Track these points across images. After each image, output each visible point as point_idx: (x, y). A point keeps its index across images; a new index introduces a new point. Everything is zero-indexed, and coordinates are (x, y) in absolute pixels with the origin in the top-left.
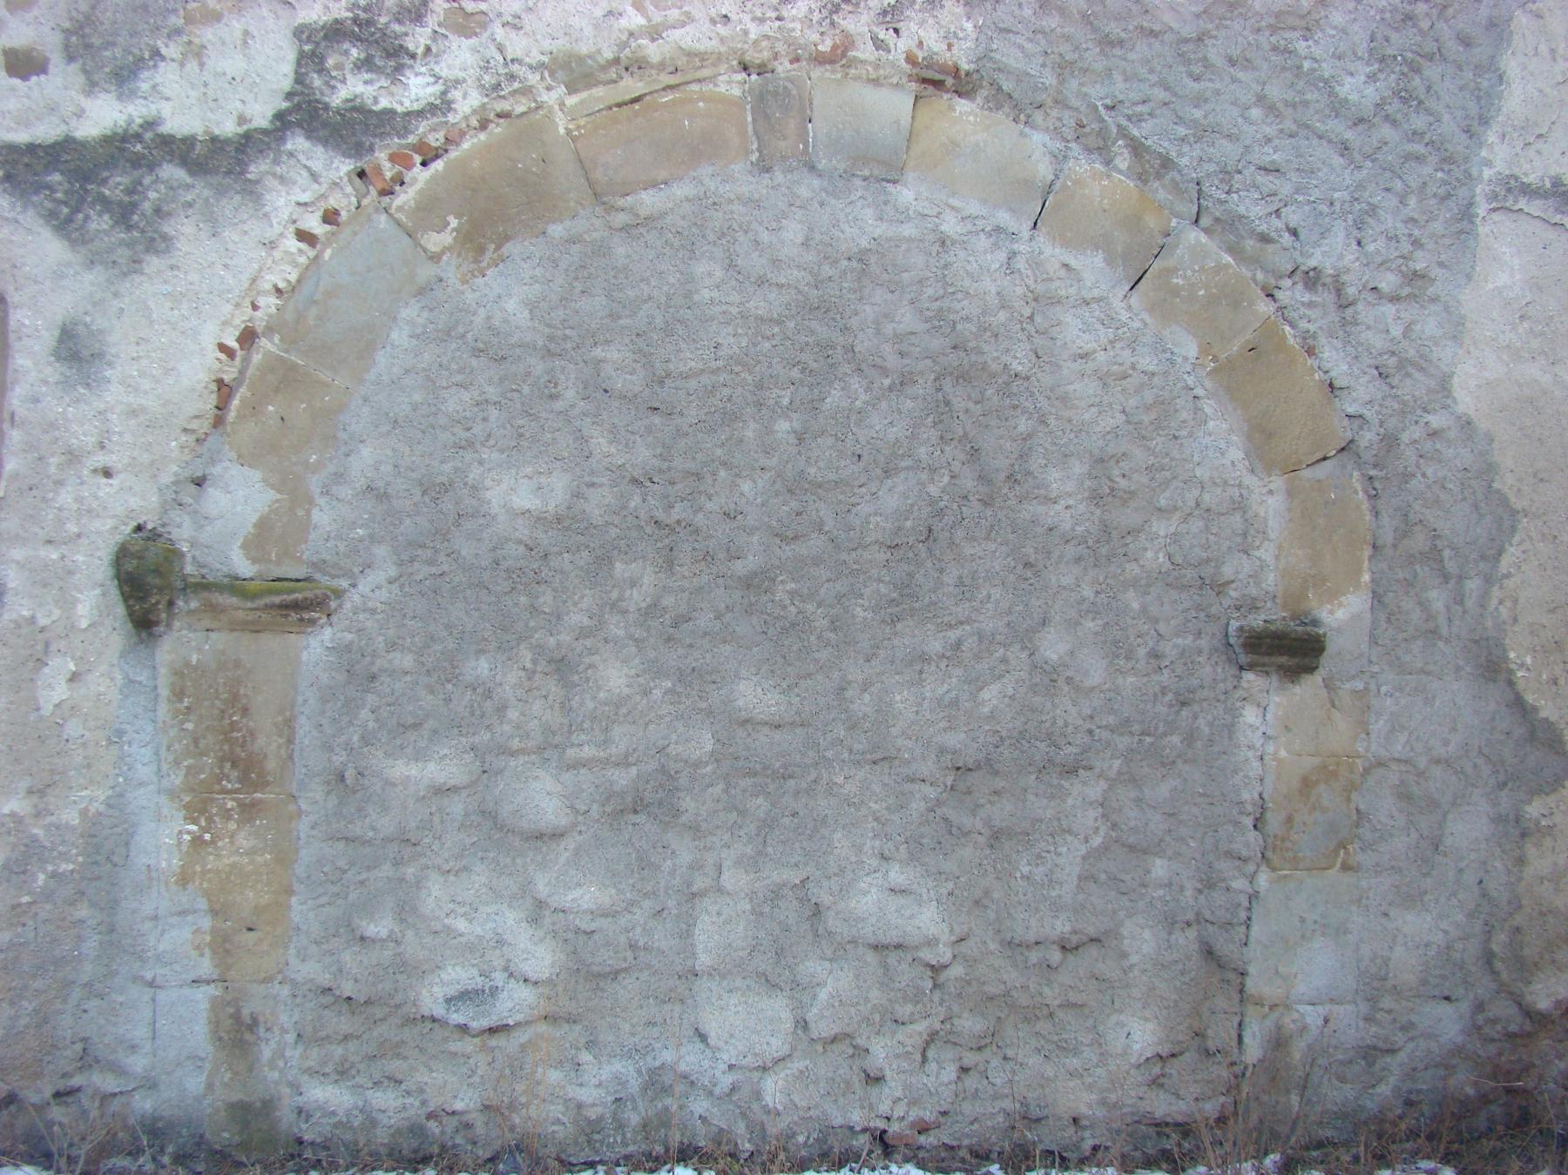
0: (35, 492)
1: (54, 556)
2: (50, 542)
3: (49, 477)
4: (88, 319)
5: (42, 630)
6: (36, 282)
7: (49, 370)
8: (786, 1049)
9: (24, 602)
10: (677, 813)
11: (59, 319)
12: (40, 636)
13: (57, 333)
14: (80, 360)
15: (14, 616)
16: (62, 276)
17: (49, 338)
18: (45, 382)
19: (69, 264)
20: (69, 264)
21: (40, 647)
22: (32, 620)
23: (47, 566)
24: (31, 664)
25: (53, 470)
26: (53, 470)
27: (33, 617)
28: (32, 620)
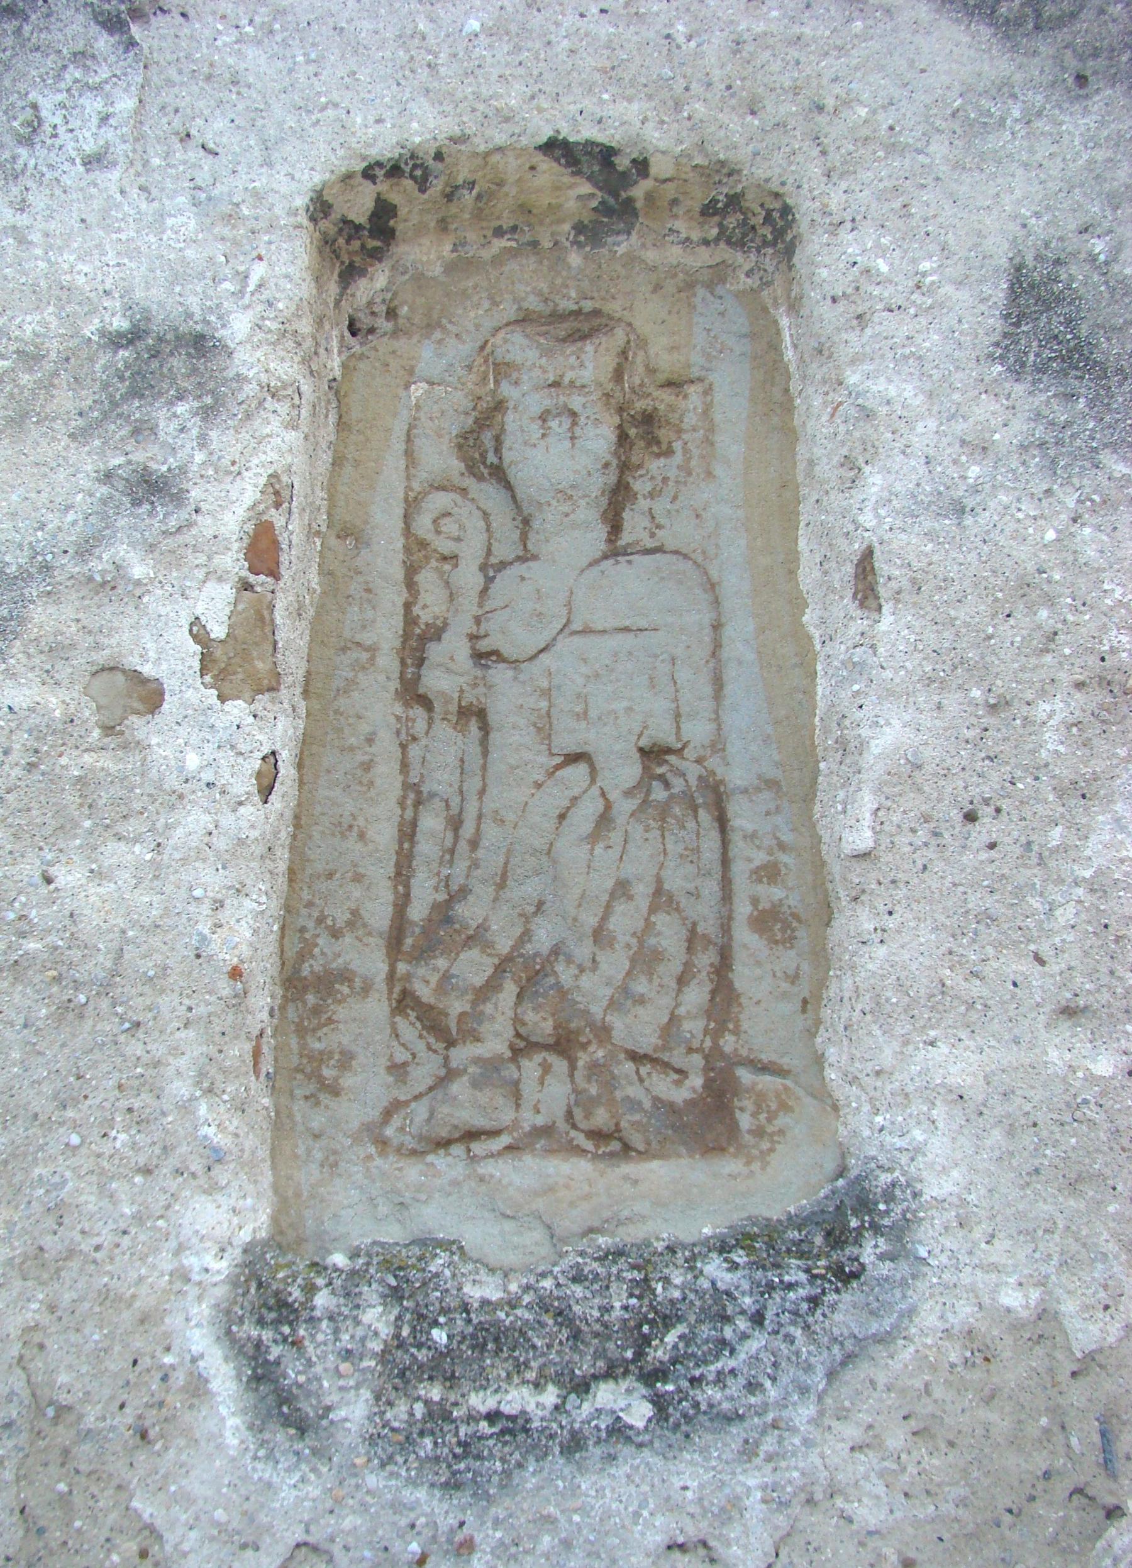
0: (987, 828)
1: (1104, 1066)
2: (1069, 1012)
3: (1036, 771)
4: (1099, 246)
5: (1087, 1365)
6: (892, 149)
7: (986, 409)
8: (530, 546)
9: (997, 1252)
10: (531, 31)
11: (1000, 253)
12: (1076, 1395)
13: (999, 292)
14: (1096, 370)
15: (964, 1312)
16: (985, 126)
17: (974, 310)
18: (982, 449)
19: (1004, 89)
20: (1004, 89)
21: (1083, 1438)
22: (1042, 1328)
23: (1075, 1106)
24: (1051, 1514)
25: (1051, 741)
26: (1051, 741)
27: (1045, 1314)
28: (1042, 1328)
